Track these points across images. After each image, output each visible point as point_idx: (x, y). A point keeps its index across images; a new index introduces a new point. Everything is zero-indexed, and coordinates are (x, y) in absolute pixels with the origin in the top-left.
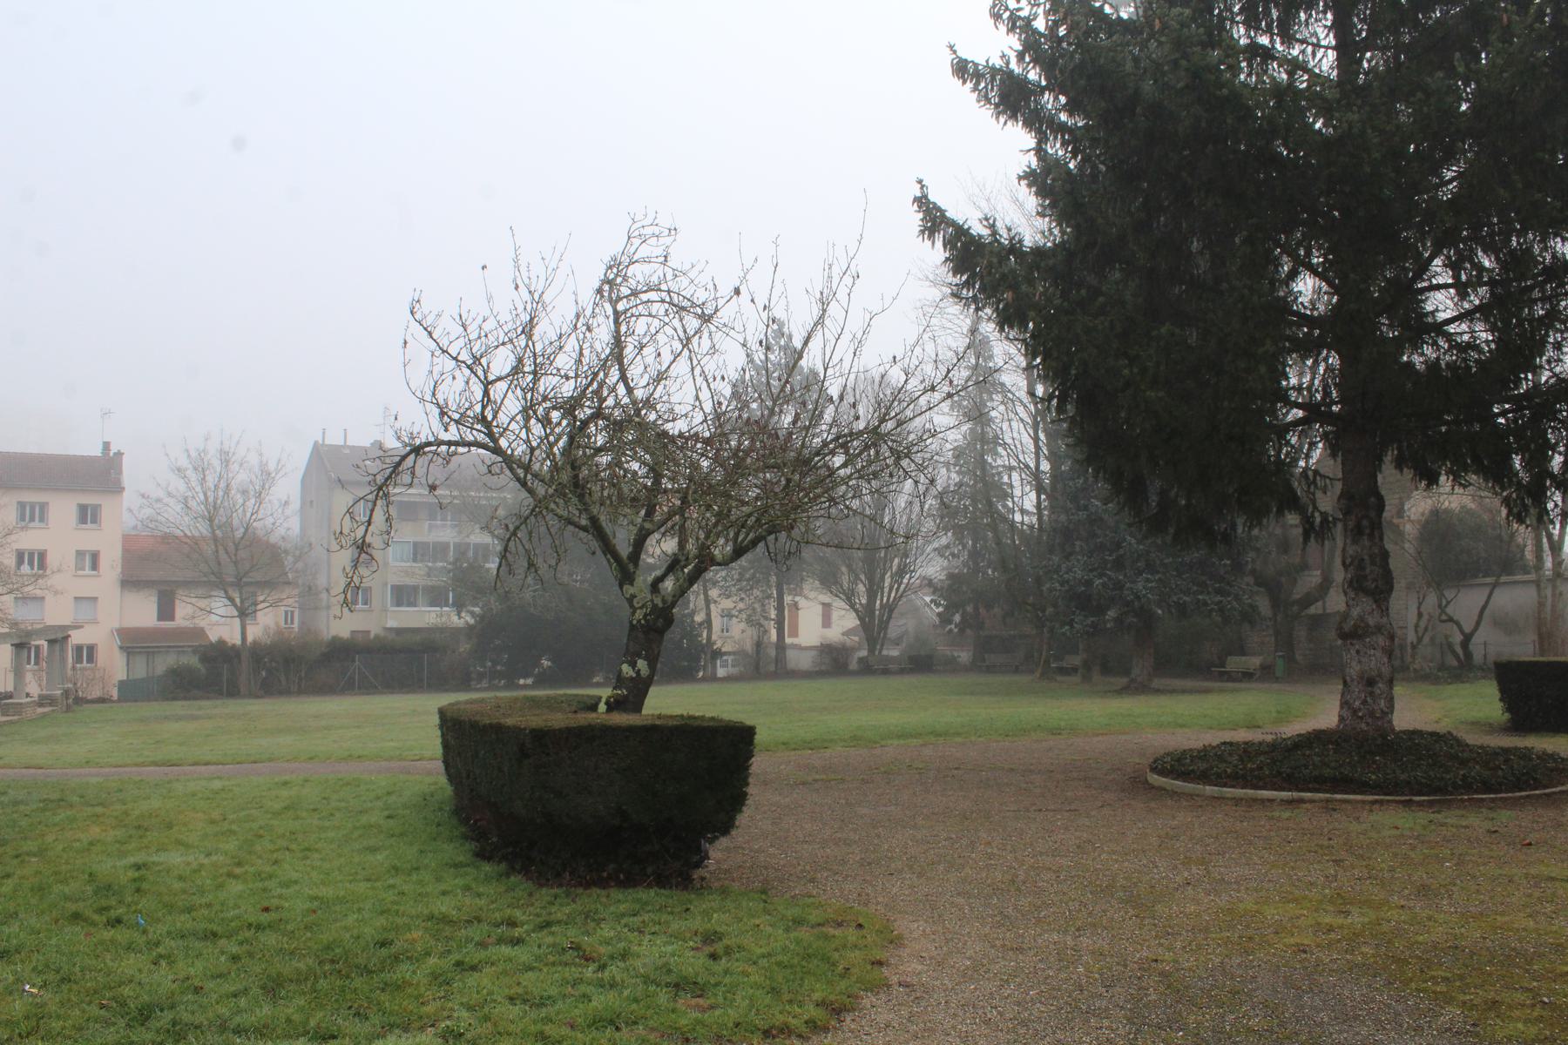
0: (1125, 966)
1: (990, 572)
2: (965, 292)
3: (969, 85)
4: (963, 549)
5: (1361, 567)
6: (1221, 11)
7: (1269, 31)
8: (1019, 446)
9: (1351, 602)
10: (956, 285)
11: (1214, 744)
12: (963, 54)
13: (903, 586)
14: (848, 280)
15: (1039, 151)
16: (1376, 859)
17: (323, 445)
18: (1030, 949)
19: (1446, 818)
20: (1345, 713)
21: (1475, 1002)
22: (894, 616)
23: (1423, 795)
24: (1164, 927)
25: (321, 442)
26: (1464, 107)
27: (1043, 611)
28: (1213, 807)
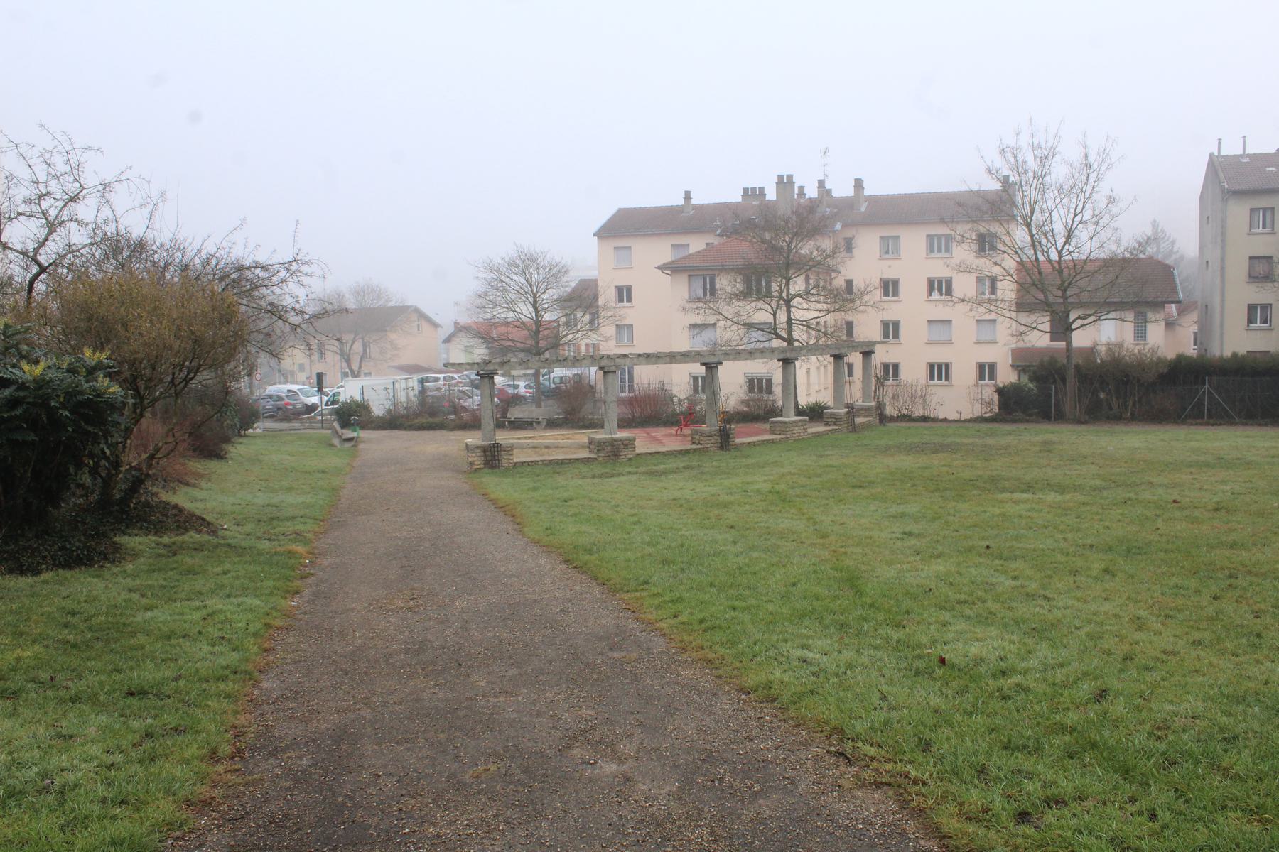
17: (1219, 156)
25: (1216, 154)
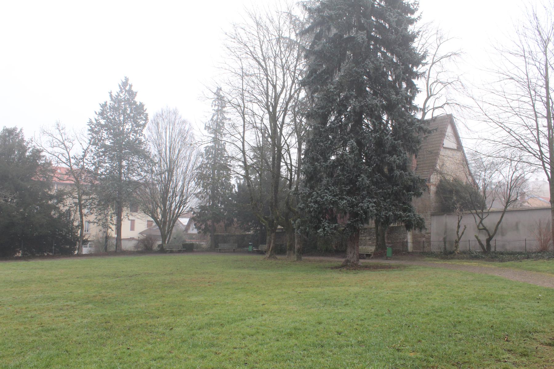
22: (175, 225)
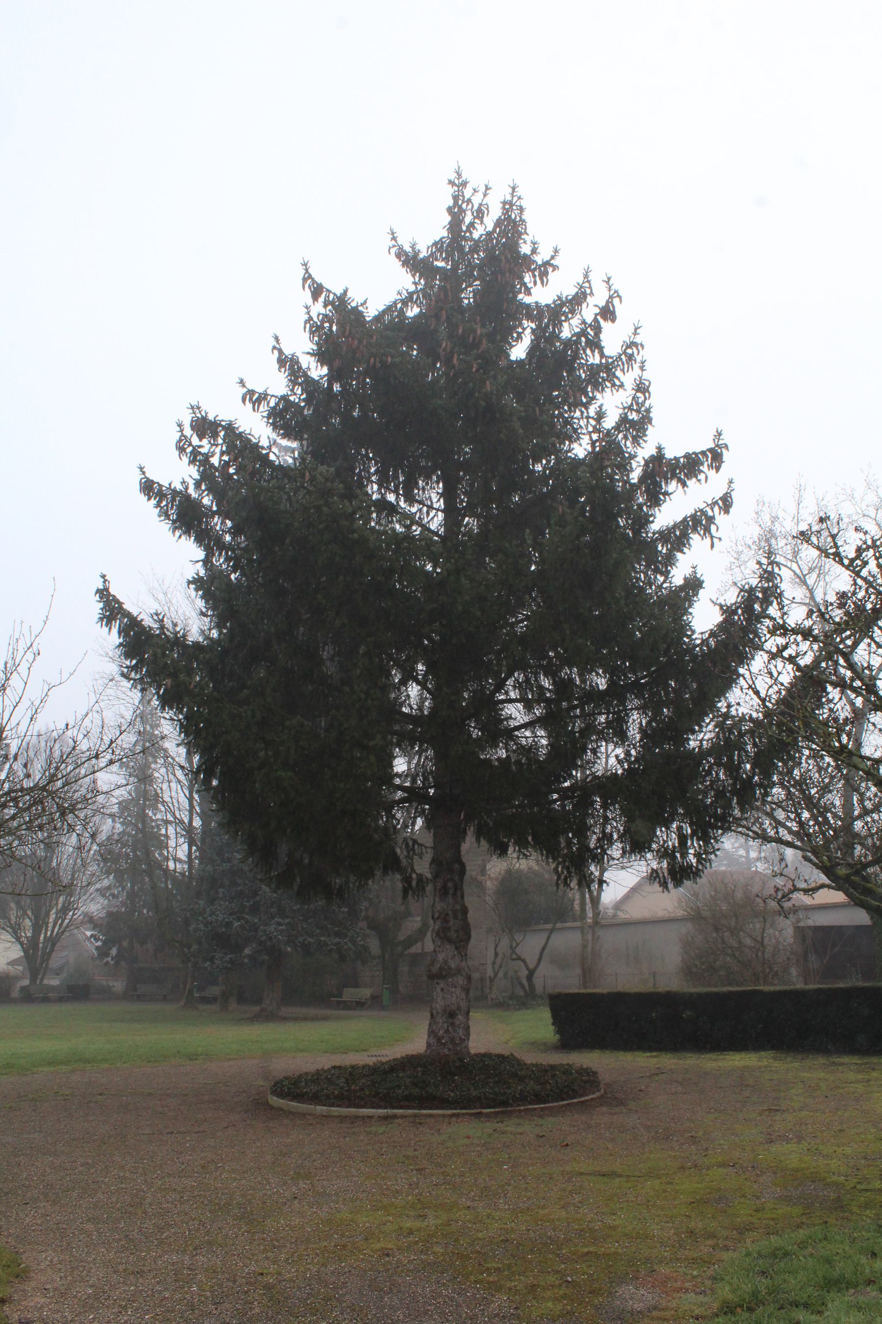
0: (235, 1281)
1: (145, 911)
2: (133, 674)
3: (153, 502)
4: (123, 890)
5: (446, 921)
6: (360, 471)
7: (396, 491)
8: (176, 804)
9: (437, 949)
10: (127, 667)
11: (326, 1068)
12: (151, 475)
13: (67, 921)
14: (30, 656)
15: (206, 562)
16: (451, 1166)
18: (150, 1271)
19: (507, 1126)
20: (433, 1041)
21: (518, 1288)
22: (56, 948)
23: (490, 1108)
24: (272, 1240)
26: (533, 568)
27: (189, 948)
28: (323, 1125)
